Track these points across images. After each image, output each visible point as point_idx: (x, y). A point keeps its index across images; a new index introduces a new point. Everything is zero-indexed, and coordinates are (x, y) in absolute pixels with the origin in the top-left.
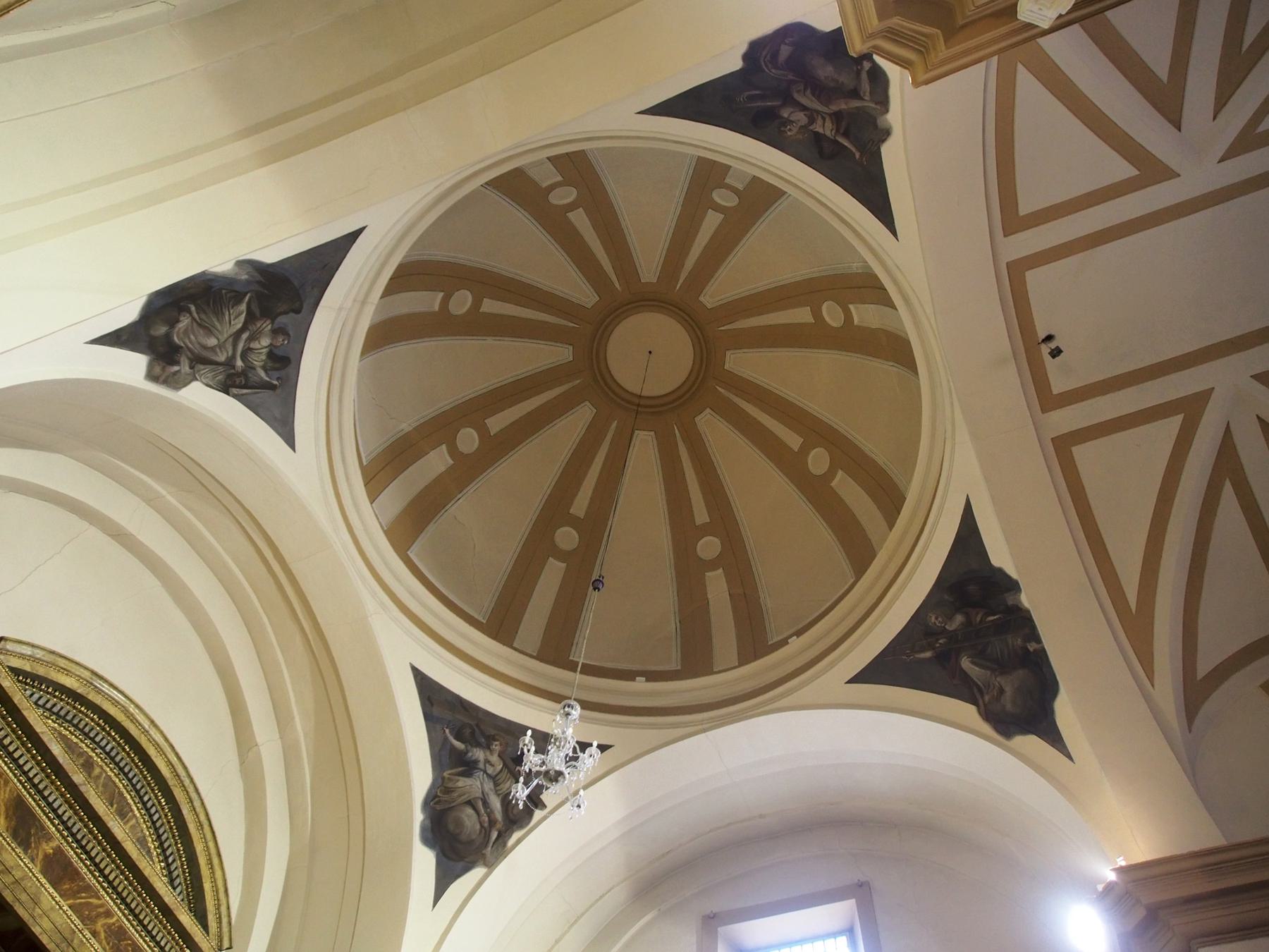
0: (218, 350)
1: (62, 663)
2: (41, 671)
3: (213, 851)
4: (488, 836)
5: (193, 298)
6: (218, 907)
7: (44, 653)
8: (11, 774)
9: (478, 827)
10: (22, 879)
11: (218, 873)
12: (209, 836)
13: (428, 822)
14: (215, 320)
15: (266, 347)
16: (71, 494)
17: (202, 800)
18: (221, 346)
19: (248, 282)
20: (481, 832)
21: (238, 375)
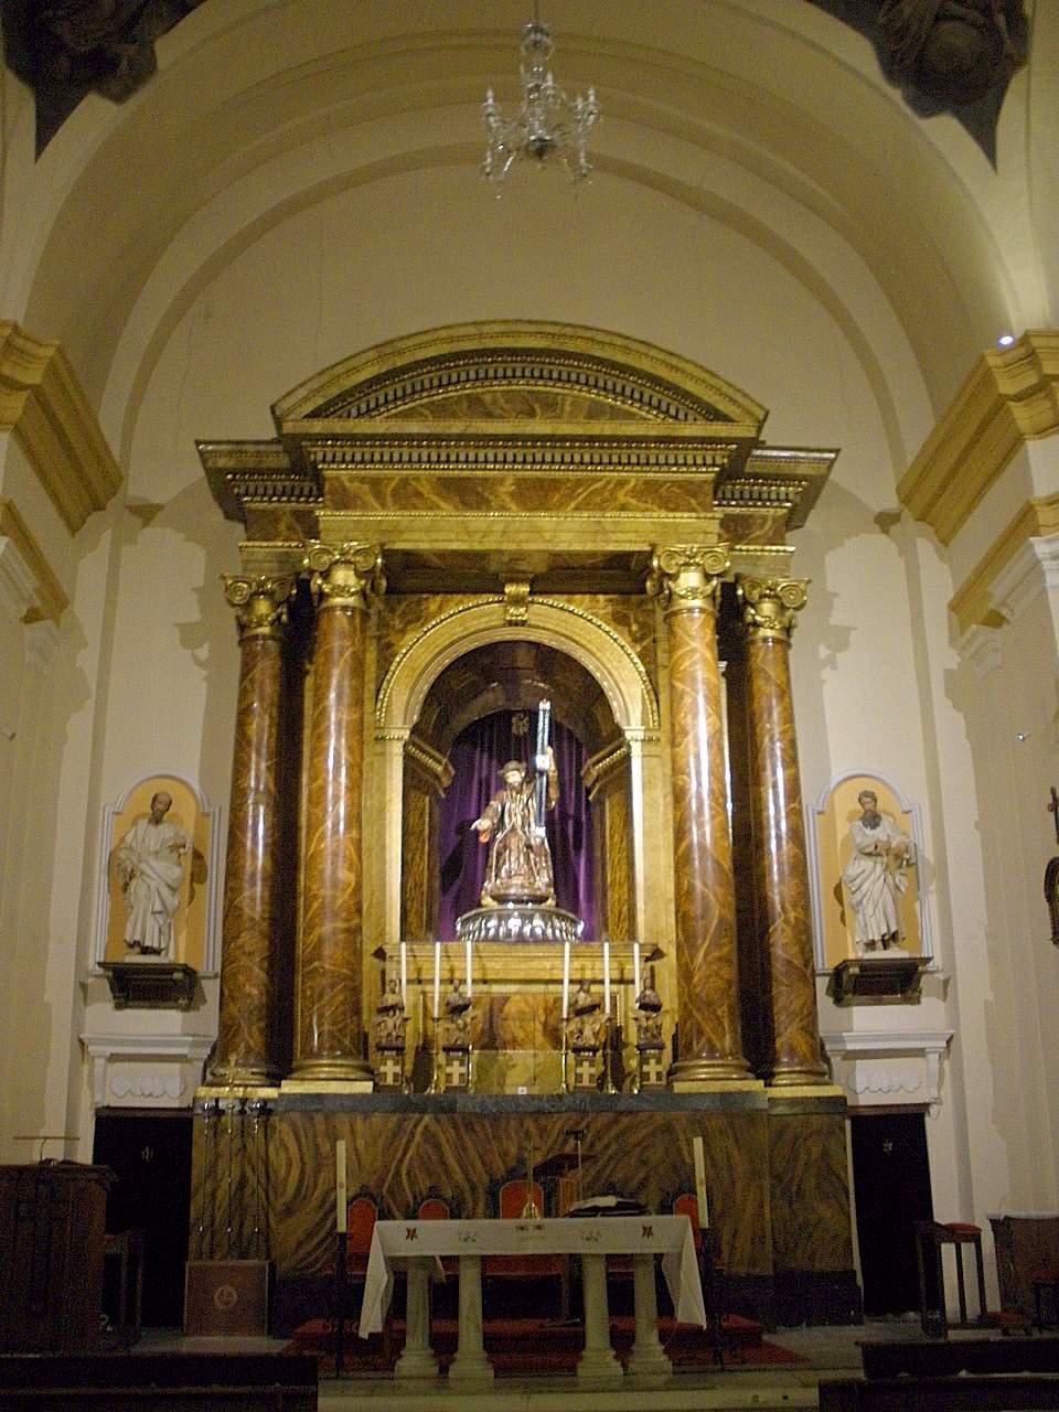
1: (340, 369)
2: (334, 391)
3: (662, 356)
4: (992, 28)
8: (414, 472)
10: (506, 527)
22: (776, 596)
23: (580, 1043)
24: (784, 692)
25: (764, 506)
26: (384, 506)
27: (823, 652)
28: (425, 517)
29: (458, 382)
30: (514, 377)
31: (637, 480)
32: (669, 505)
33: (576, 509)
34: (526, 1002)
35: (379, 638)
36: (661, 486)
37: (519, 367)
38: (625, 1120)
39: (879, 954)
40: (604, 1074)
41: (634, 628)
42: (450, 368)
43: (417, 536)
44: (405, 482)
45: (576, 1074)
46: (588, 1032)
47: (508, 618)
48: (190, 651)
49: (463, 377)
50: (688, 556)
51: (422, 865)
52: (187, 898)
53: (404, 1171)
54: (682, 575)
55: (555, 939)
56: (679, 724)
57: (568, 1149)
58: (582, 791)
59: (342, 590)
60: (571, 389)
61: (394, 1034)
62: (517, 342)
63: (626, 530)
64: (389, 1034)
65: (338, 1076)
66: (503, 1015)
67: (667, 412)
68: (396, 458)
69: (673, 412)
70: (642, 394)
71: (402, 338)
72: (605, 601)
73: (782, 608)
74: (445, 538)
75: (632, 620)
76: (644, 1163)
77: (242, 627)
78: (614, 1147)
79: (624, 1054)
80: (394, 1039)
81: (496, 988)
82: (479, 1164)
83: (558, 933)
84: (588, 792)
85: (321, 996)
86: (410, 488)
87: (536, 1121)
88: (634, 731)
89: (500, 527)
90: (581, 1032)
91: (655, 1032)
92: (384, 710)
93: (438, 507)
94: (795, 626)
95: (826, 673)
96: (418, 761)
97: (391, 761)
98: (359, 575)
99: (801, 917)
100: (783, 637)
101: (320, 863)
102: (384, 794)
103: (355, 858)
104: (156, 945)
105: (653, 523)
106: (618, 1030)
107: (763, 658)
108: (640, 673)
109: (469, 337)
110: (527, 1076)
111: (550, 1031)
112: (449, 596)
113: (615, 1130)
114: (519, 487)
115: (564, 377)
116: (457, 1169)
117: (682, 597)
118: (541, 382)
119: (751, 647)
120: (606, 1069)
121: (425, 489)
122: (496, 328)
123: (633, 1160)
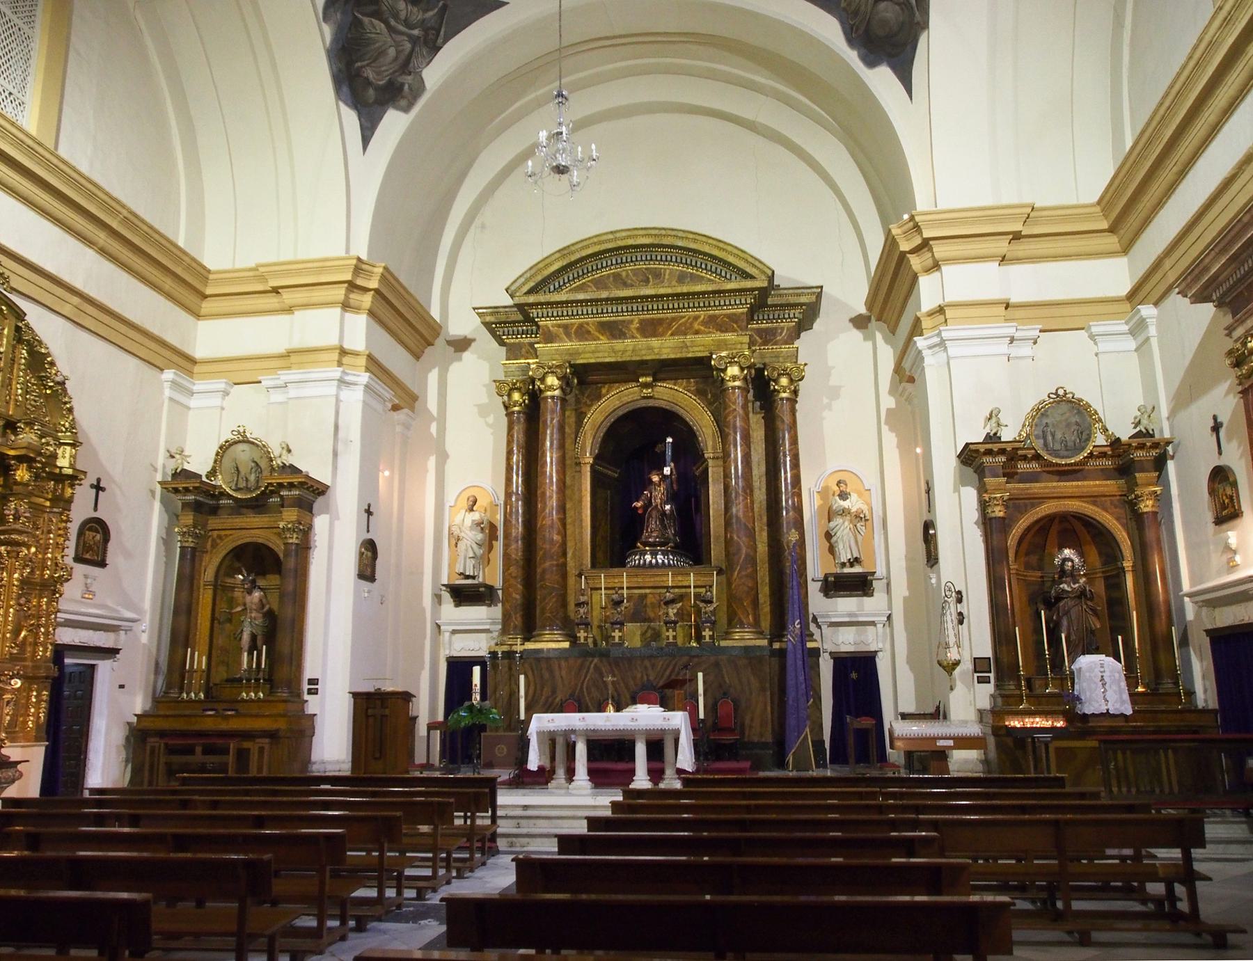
0: (401, 48)
2: (539, 278)
3: (714, 242)
5: (349, 64)
9: (897, 7)
11: (729, 248)
13: (864, 51)
14: (372, 47)
15: (407, 5)
16: (499, 169)
17: (681, 230)
18: (397, 45)
19: (343, 13)
20: (902, 9)
21: (426, 34)
25: (782, 322)
26: (571, 341)
27: (825, 401)
28: (591, 345)
29: (607, 266)
30: (637, 260)
32: (723, 328)
33: (672, 335)
35: (576, 410)
37: (639, 255)
38: (696, 660)
39: (847, 570)
42: (601, 259)
43: (587, 355)
44: (581, 326)
49: (609, 263)
50: (731, 358)
54: (729, 369)
59: (551, 388)
60: (669, 265)
63: (698, 344)
64: (582, 617)
67: (721, 275)
68: (575, 313)
69: (723, 274)
70: (706, 265)
71: (573, 245)
73: (791, 381)
77: (506, 407)
83: (671, 562)
86: (583, 329)
89: (631, 348)
93: (599, 339)
98: (558, 379)
100: (793, 397)
104: (472, 574)
114: (641, 324)
115: (664, 258)
117: (729, 381)
118: (652, 263)
121: (592, 329)
122: (624, 234)
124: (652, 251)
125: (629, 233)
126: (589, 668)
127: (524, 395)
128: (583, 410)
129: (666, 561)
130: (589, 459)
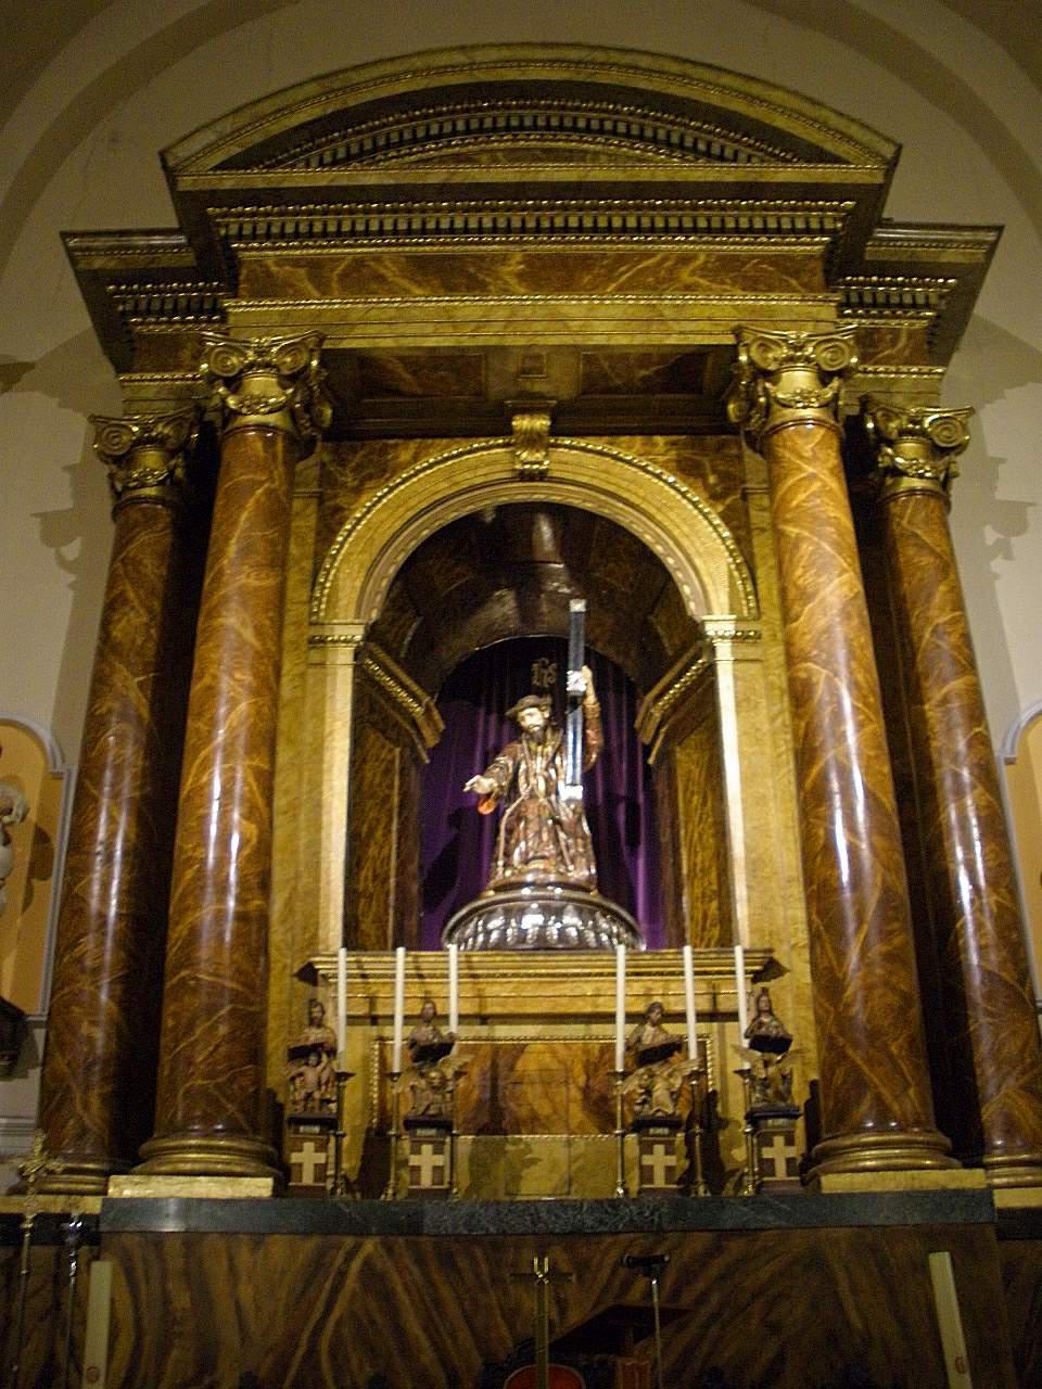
1: (267, 107)
3: (737, 83)
6: (825, 127)
7: (231, 119)
10: (513, 315)
12: (708, 75)
22: (923, 433)
23: (648, 1111)
24: (947, 566)
25: (894, 316)
28: (388, 305)
31: (708, 256)
32: (752, 284)
34: (554, 1053)
35: (321, 499)
36: (744, 264)
40: (690, 1171)
41: (712, 479)
43: (371, 330)
44: (359, 263)
45: (641, 1167)
46: (660, 1091)
47: (518, 467)
48: (53, 550)
51: (388, 849)
52: (20, 898)
53: (324, 1345)
55: (600, 945)
56: (795, 585)
57: (634, 1296)
58: (635, 749)
59: (254, 404)
61: (317, 1095)
62: (524, 74)
64: (309, 1096)
65: (211, 1167)
66: (514, 1076)
72: (666, 444)
74: (418, 332)
75: (708, 470)
76: (774, 1328)
78: (715, 1299)
79: (721, 1138)
80: (317, 1104)
81: (502, 1031)
82: (464, 1335)
83: (604, 938)
84: (647, 750)
85: (191, 1027)
87: (497, 928)
88: (719, 624)
90: (649, 1092)
91: (781, 1087)
92: (324, 599)
94: (956, 475)
95: (998, 565)
96: (381, 688)
97: (335, 674)
99: (1007, 903)
100: (938, 489)
101: (202, 806)
102: (322, 720)
103: (260, 802)
105: (735, 307)
106: (711, 1099)
107: (909, 518)
108: (724, 540)
109: (453, 68)
110: (556, 1177)
111: (595, 1103)
112: (430, 441)
113: (715, 1269)
116: (425, 1343)
119: (892, 504)
120: (692, 1165)
122: (494, 54)
123: (755, 1321)
124: (564, 108)
125: (506, 53)
126: (342, 1274)
127: (173, 454)
128: (341, 501)
129: (591, 935)
130: (349, 630)
